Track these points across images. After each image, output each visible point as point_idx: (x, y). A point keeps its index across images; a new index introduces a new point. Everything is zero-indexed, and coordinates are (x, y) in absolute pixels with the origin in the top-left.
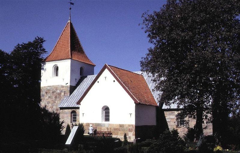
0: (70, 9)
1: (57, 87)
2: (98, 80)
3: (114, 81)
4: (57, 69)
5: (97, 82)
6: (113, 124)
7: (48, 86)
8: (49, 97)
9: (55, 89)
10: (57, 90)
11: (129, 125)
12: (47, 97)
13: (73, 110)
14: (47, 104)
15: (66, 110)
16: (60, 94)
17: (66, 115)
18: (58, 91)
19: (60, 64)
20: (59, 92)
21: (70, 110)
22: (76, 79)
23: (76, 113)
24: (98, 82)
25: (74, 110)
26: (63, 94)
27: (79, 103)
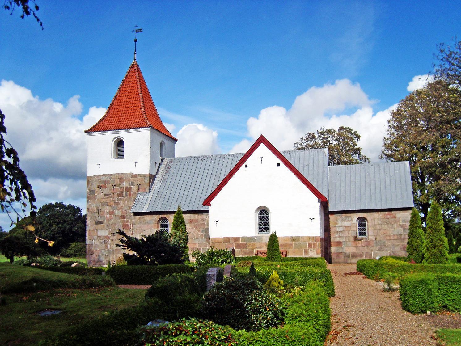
0: (136, 41)
1: (122, 176)
2: (246, 163)
3: (278, 165)
4: (120, 143)
5: (244, 166)
6: (219, 238)
7: (104, 175)
8: (106, 195)
9: (117, 181)
10: (121, 181)
11: (309, 238)
12: (102, 195)
13: (161, 216)
14: (100, 208)
15: (147, 218)
16: (128, 189)
17: (146, 225)
18: (125, 184)
19: (127, 136)
20: (128, 185)
21: (156, 217)
22: (156, 163)
23: (167, 222)
24: (246, 166)
25: (165, 216)
26: (134, 188)
27: (207, 202)
